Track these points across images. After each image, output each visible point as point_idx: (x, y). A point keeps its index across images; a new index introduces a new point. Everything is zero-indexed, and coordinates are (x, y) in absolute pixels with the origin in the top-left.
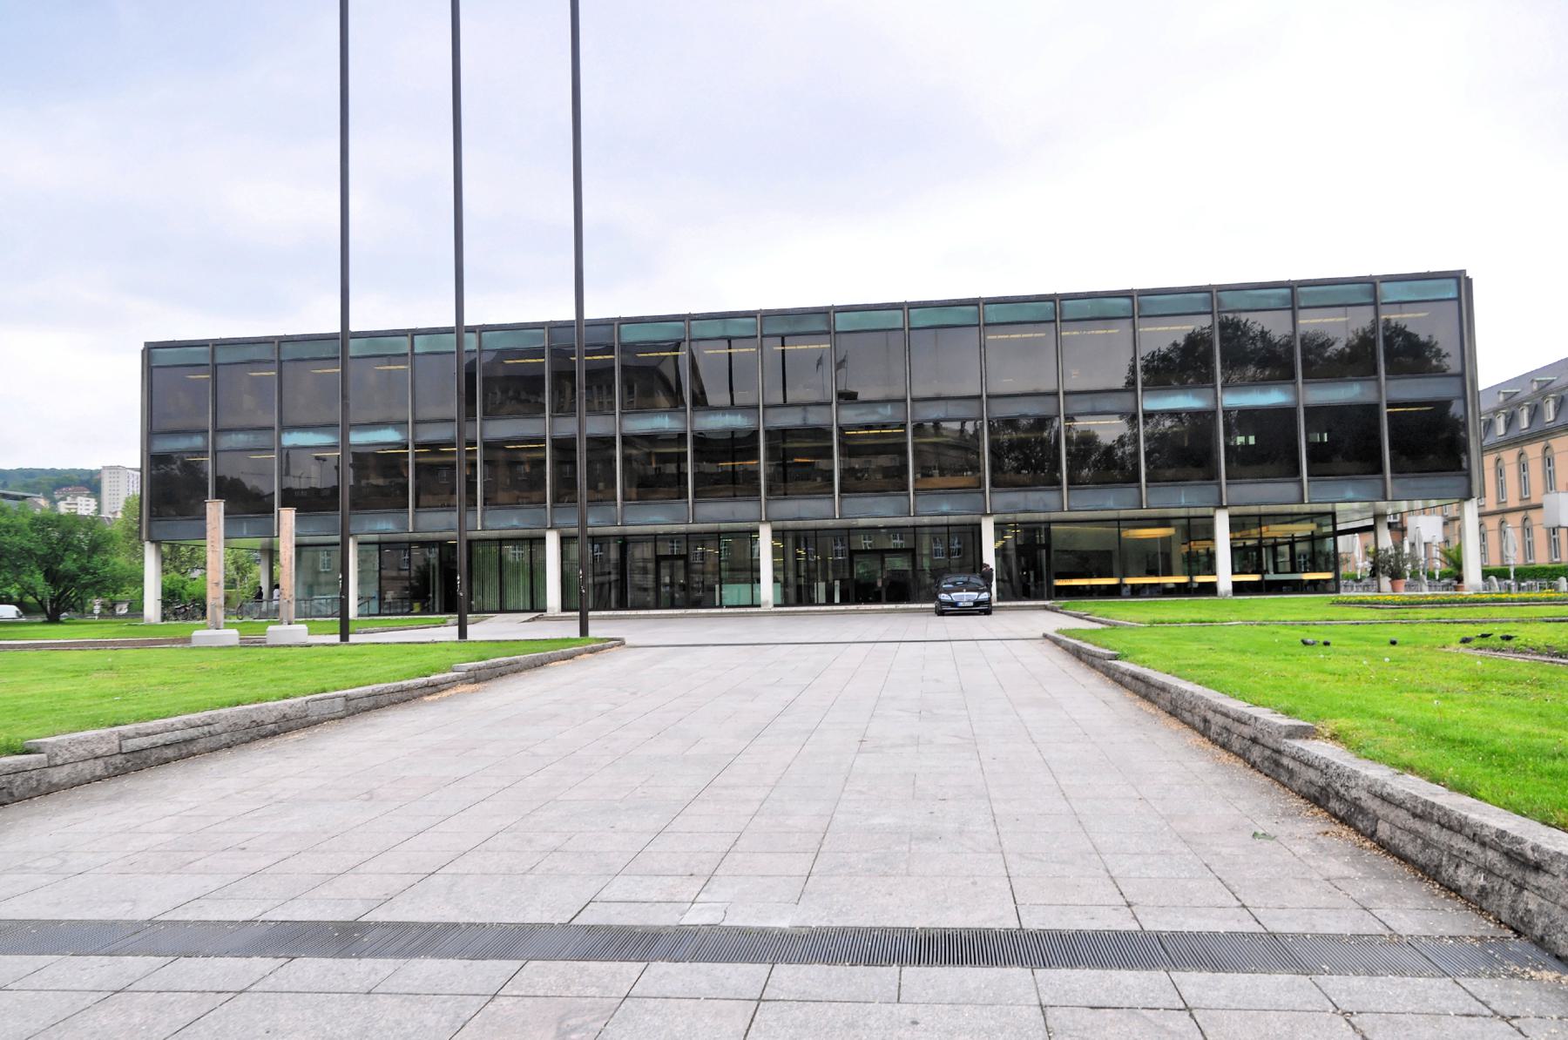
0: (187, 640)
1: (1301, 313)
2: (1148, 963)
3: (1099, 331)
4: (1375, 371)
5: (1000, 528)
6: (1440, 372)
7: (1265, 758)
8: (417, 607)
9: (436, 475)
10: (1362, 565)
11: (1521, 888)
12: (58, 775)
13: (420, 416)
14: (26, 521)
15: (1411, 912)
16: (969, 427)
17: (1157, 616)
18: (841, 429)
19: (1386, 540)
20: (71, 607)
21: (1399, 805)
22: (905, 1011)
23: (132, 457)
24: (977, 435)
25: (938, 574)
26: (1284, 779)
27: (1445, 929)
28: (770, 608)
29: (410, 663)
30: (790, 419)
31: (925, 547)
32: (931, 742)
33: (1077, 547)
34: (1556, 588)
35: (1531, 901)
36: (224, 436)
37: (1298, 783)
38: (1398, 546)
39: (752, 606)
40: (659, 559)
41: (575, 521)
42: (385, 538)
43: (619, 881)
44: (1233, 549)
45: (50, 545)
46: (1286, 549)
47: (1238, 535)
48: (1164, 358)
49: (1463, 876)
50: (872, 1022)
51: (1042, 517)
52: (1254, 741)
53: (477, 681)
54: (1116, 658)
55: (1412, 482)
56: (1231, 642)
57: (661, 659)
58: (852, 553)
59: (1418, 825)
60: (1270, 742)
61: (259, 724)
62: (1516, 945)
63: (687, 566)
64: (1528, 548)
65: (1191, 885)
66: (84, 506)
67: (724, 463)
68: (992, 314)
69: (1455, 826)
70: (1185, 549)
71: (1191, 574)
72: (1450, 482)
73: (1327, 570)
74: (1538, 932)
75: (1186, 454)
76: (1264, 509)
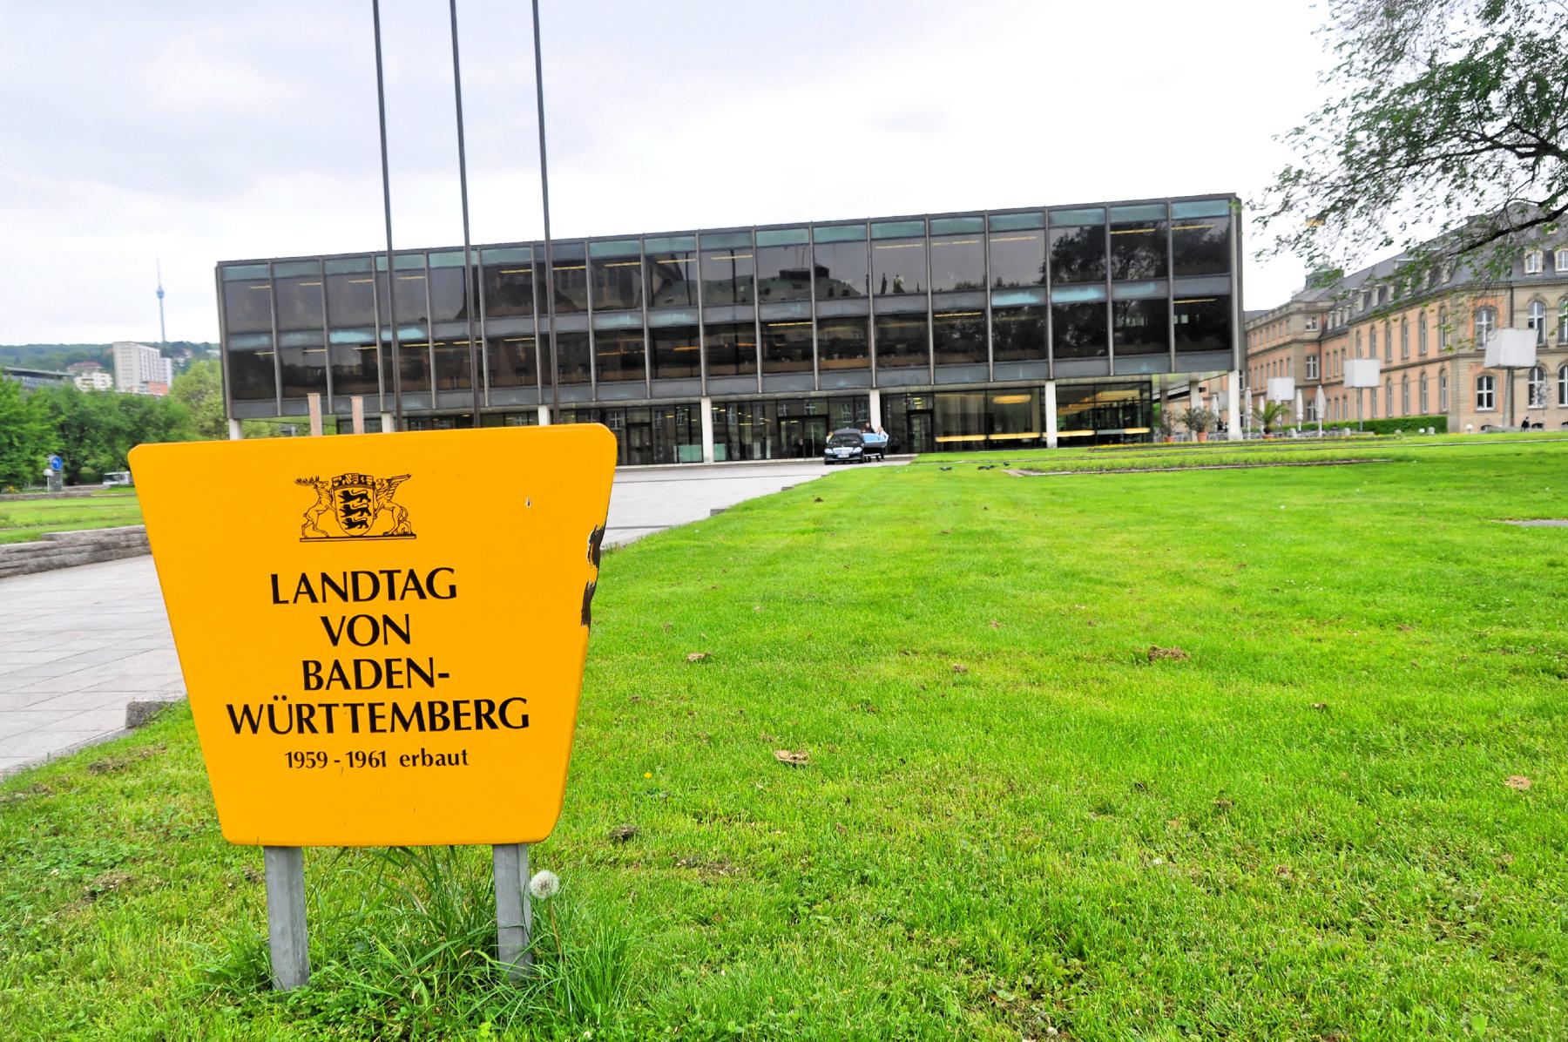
13: (283, 326)
55: (1191, 358)
71: (1095, 428)
72: (1220, 357)
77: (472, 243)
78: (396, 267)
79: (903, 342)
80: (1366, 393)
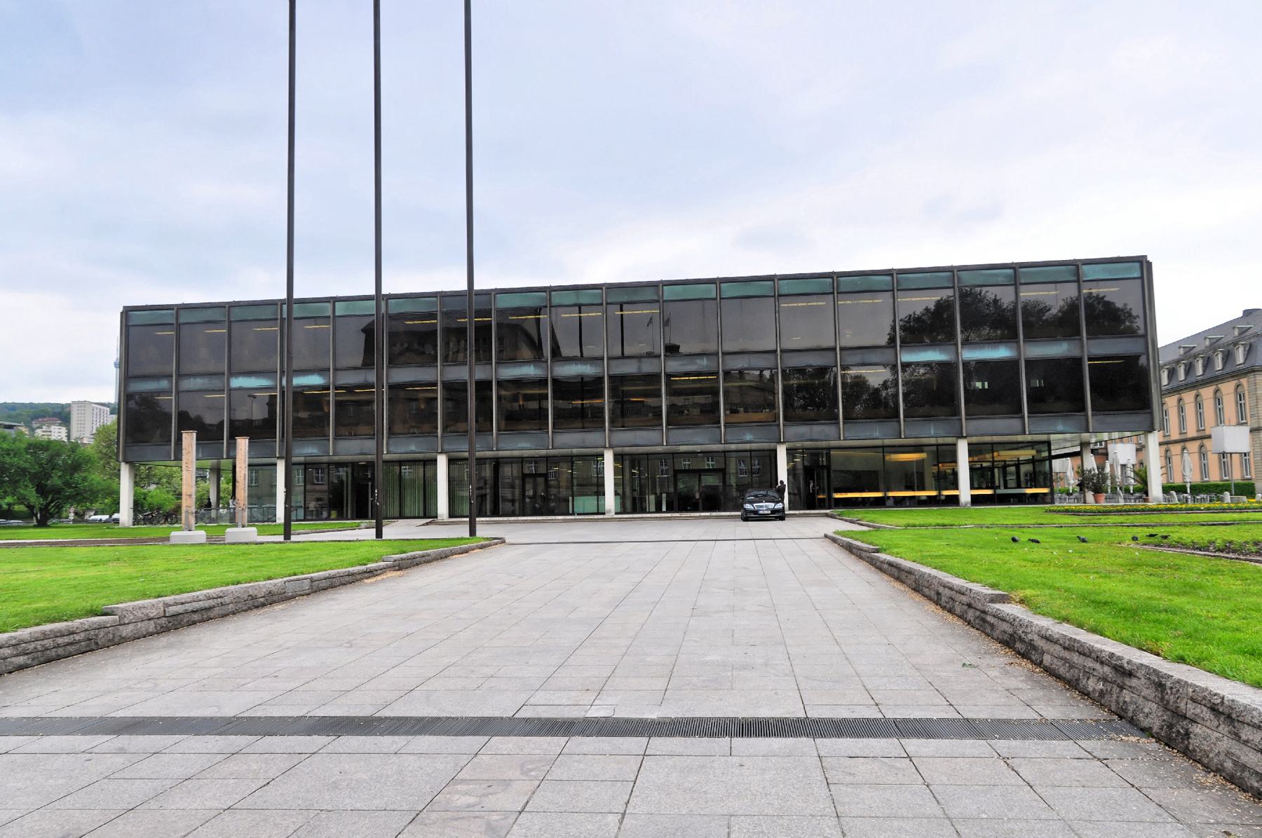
0: (168, 539)
1: (1022, 288)
2: (887, 735)
3: (866, 301)
4: (1078, 333)
5: (791, 453)
6: (1131, 333)
7: (975, 617)
8: (334, 514)
9: (354, 411)
10: (1072, 481)
11: (1122, 688)
12: (126, 631)
13: (339, 365)
14: (23, 446)
15: (1056, 706)
16: (767, 374)
17: (911, 522)
18: (668, 376)
19: (1090, 462)
20: (52, 516)
21: (1056, 642)
22: (734, 759)
23: (110, 394)
24: (773, 379)
25: (742, 489)
26: (988, 631)
27: (1076, 715)
28: (612, 515)
29: (350, 555)
30: (629, 368)
31: (732, 468)
32: (743, 609)
33: (852, 469)
34: (1222, 500)
35: (1127, 696)
36: (186, 378)
37: (997, 633)
38: (1101, 468)
39: (598, 513)
40: (524, 477)
41: (466, 447)
42: (310, 459)
43: (540, 694)
44: (972, 469)
45: (41, 465)
46: (1013, 469)
47: (976, 459)
48: (918, 319)
49: (1093, 685)
50: (715, 765)
51: (824, 444)
52: (969, 606)
53: (400, 569)
54: (877, 551)
56: (968, 541)
57: (530, 553)
58: (676, 472)
59: (1066, 654)
60: (979, 606)
61: (253, 598)
62: (1118, 723)
63: (547, 486)
64: (1204, 469)
65: (918, 693)
66: (57, 433)
67: (577, 402)
68: (785, 288)
69: (1087, 652)
70: (935, 469)
71: (939, 489)
72: (1140, 418)
73: (1045, 487)
74: (1130, 714)
75: (934, 396)
76: (996, 439)
77: (385, 291)
78: (295, 315)
79: (631, 400)
80: (1236, 458)
